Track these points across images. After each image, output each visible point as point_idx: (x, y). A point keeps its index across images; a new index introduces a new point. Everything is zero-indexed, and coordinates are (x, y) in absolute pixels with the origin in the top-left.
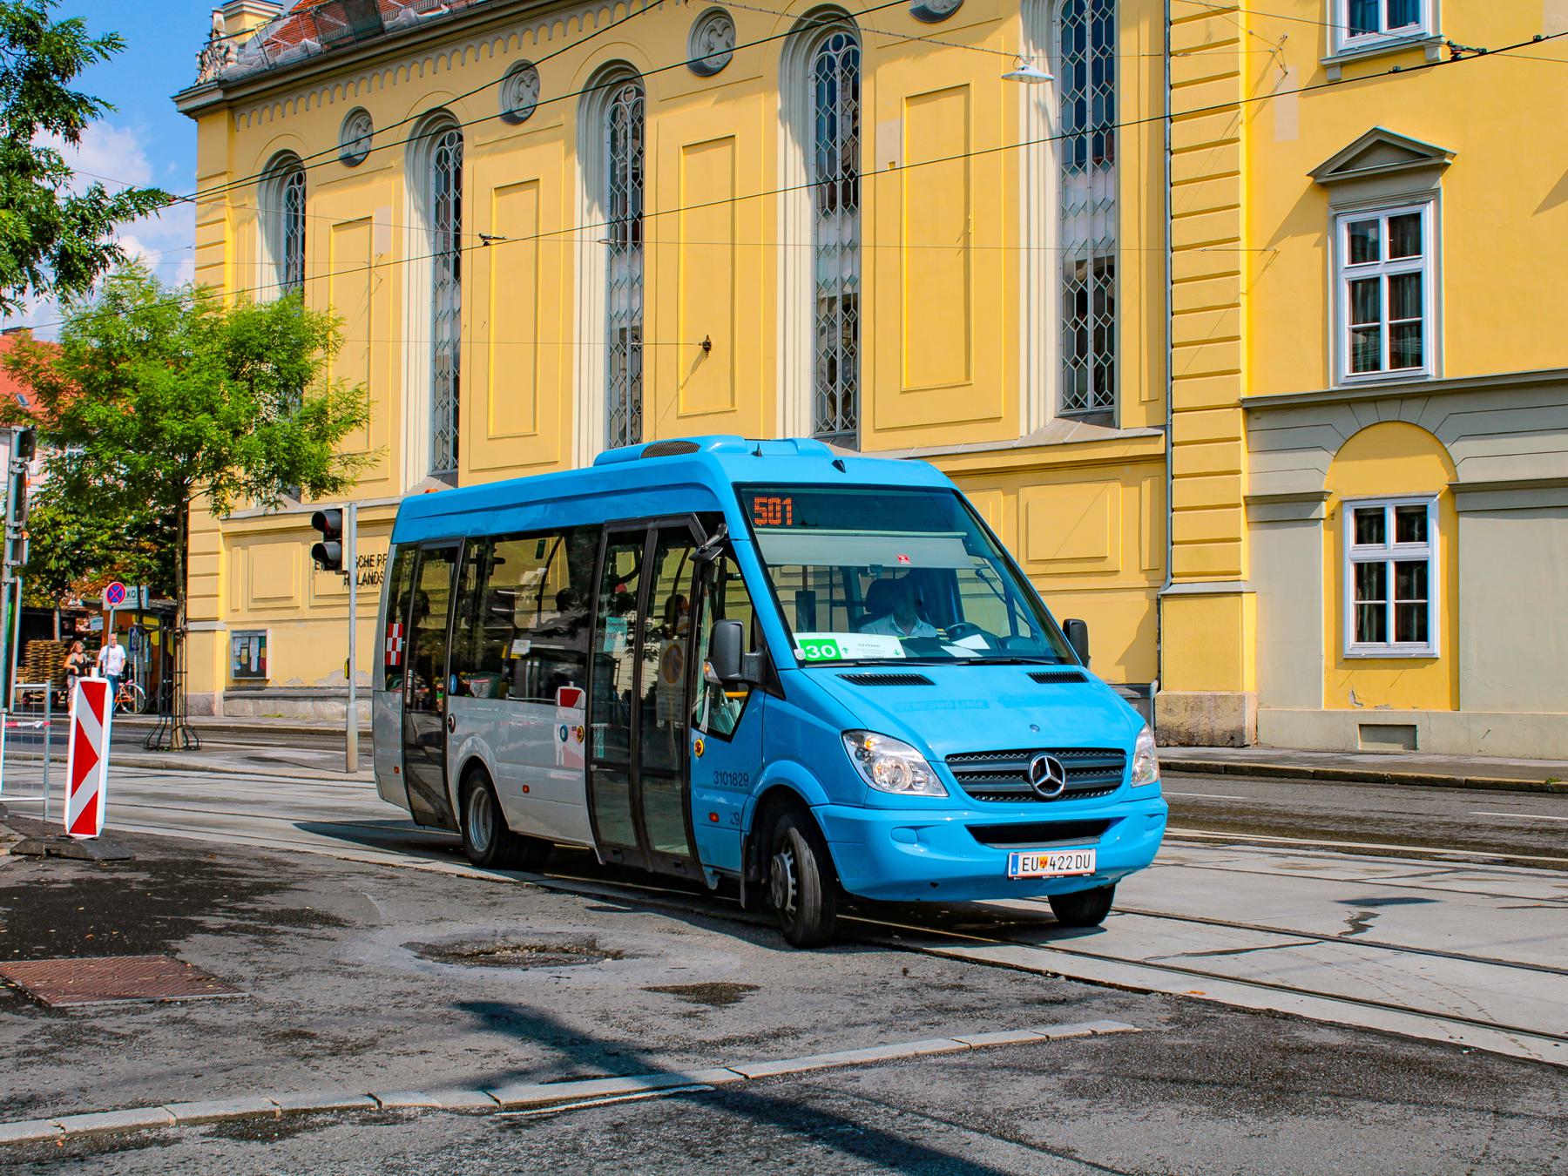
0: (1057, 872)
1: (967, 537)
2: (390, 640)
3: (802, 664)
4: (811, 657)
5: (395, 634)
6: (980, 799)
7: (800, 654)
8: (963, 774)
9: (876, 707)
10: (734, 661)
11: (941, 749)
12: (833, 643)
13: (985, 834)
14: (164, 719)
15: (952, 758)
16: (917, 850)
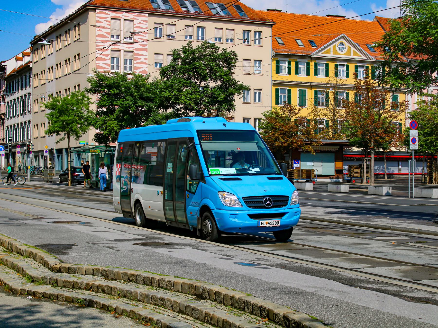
0: (270, 225)
1: (258, 143)
2: (117, 168)
3: (210, 175)
4: (213, 174)
5: (118, 167)
6: (251, 208)
7: (210, 173)
8: (247, 202)
9: (227, 186)
10: (194, 174)
11: (241, 196)
12: (219, 170)
13: (252, 216)
14: (347, 172)
15: (244, 198)
16: (236, 220)
